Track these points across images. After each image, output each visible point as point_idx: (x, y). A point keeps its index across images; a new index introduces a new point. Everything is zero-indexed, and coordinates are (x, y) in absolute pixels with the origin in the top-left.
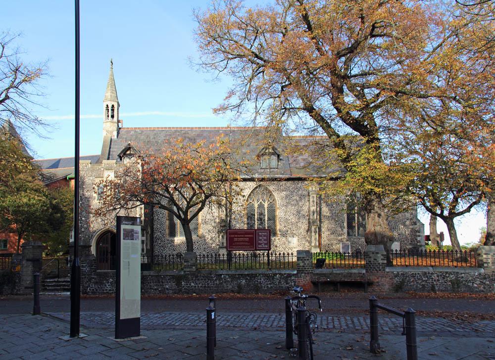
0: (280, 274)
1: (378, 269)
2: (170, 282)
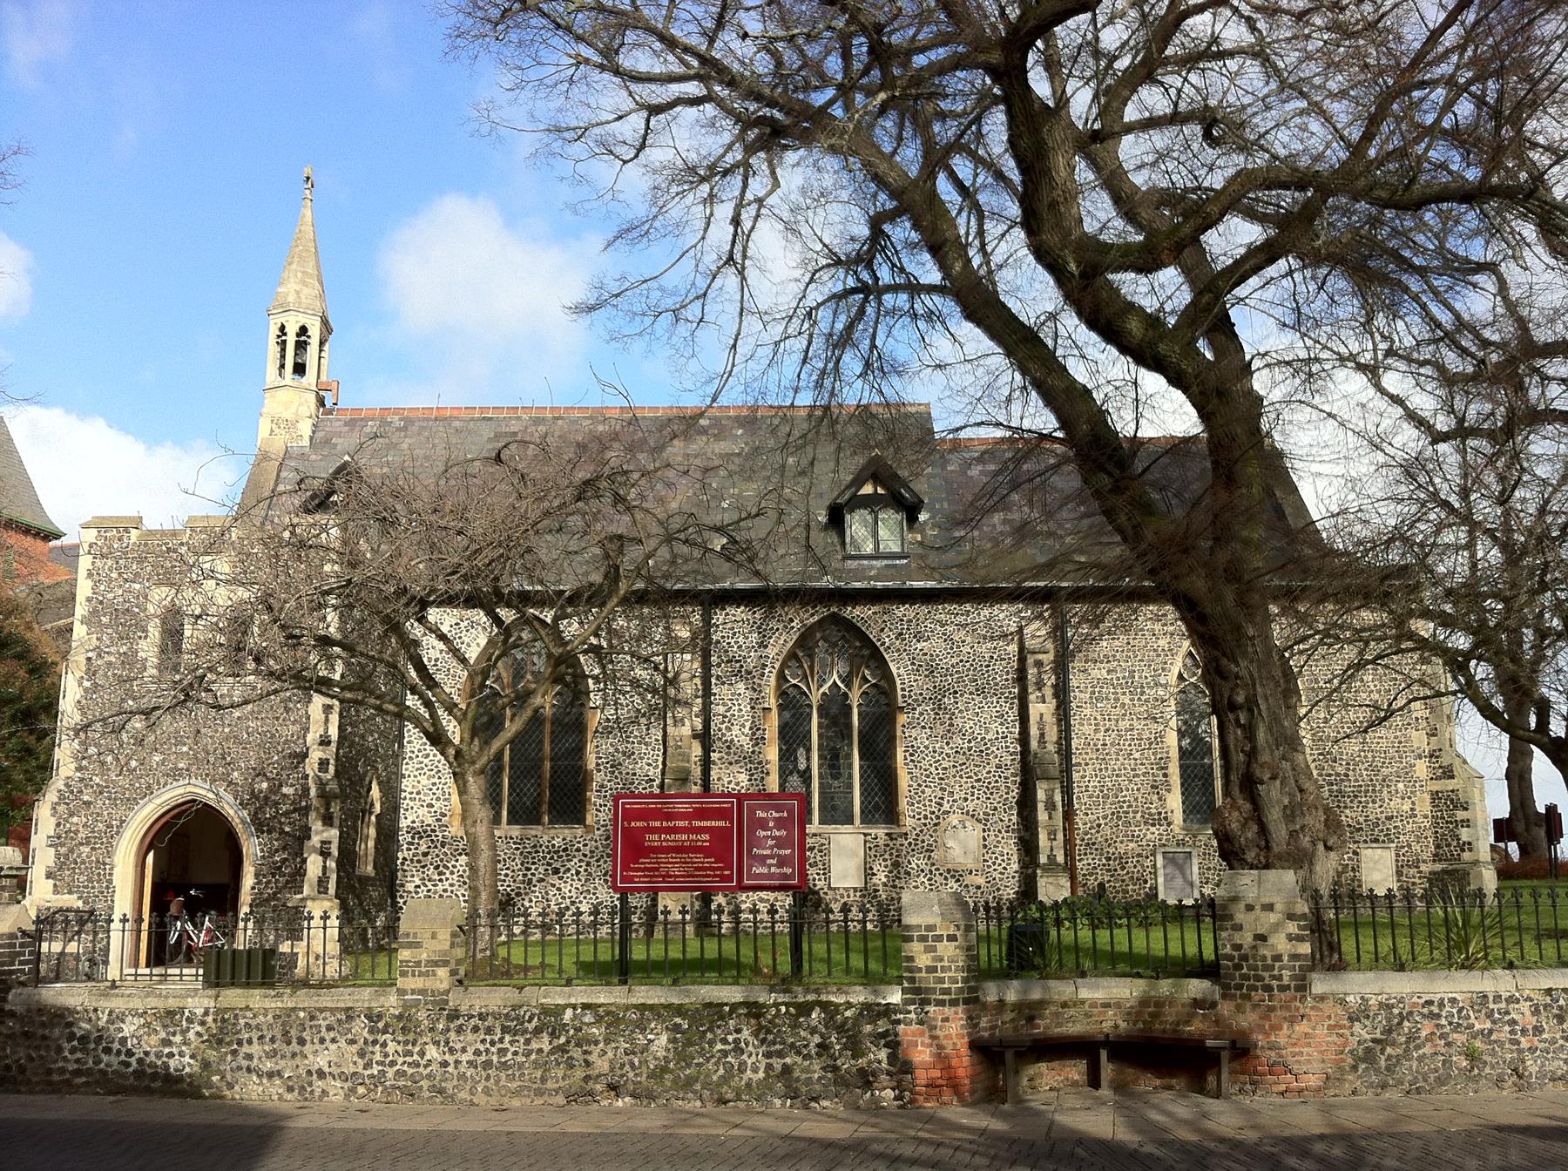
1: (1275, 983)
2: (333, 1040)
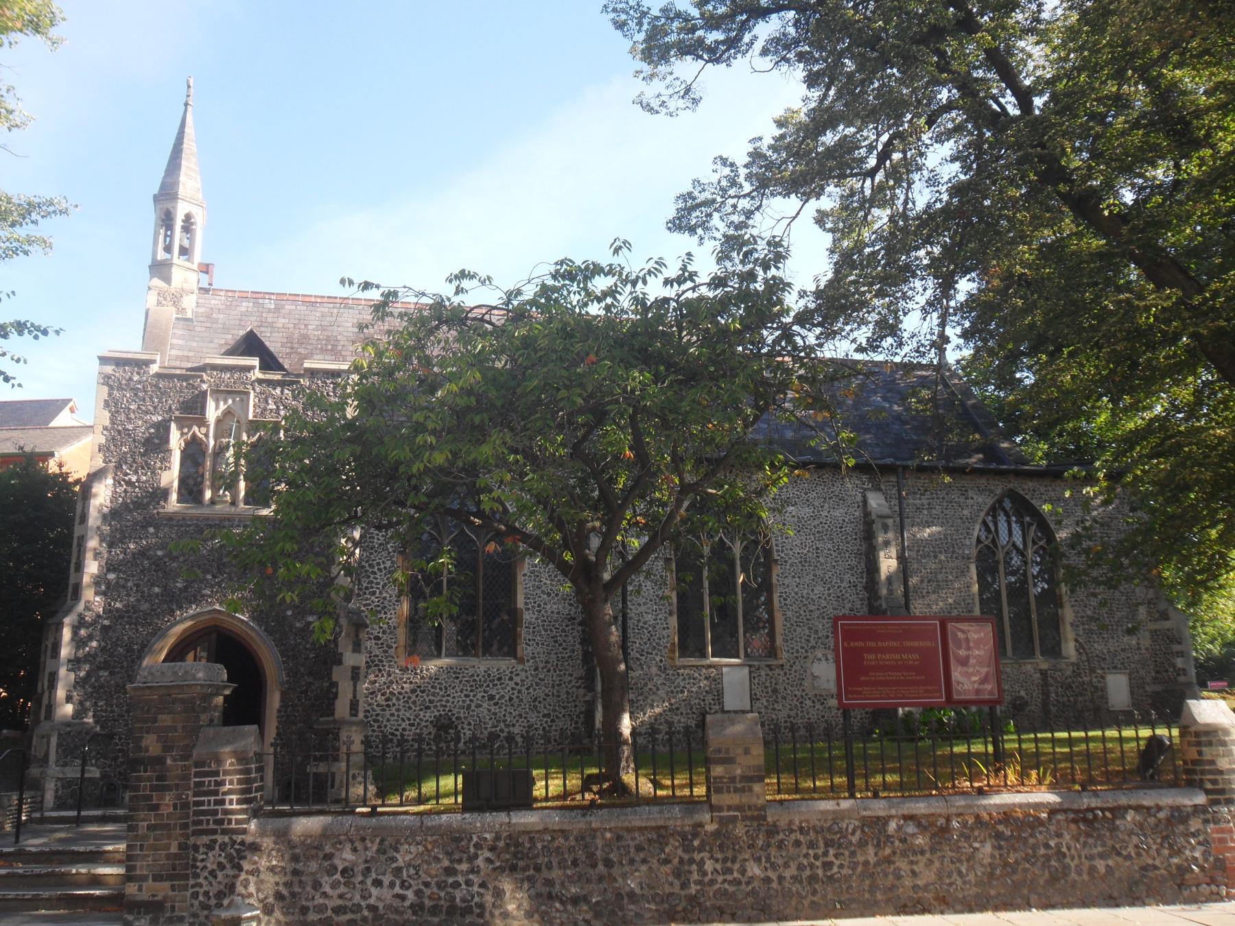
0: (1138, 808)
2: (644, 861)
